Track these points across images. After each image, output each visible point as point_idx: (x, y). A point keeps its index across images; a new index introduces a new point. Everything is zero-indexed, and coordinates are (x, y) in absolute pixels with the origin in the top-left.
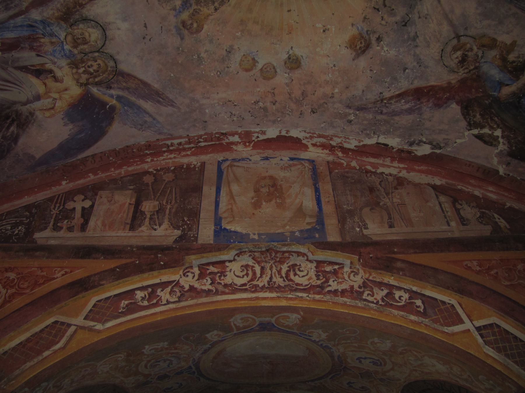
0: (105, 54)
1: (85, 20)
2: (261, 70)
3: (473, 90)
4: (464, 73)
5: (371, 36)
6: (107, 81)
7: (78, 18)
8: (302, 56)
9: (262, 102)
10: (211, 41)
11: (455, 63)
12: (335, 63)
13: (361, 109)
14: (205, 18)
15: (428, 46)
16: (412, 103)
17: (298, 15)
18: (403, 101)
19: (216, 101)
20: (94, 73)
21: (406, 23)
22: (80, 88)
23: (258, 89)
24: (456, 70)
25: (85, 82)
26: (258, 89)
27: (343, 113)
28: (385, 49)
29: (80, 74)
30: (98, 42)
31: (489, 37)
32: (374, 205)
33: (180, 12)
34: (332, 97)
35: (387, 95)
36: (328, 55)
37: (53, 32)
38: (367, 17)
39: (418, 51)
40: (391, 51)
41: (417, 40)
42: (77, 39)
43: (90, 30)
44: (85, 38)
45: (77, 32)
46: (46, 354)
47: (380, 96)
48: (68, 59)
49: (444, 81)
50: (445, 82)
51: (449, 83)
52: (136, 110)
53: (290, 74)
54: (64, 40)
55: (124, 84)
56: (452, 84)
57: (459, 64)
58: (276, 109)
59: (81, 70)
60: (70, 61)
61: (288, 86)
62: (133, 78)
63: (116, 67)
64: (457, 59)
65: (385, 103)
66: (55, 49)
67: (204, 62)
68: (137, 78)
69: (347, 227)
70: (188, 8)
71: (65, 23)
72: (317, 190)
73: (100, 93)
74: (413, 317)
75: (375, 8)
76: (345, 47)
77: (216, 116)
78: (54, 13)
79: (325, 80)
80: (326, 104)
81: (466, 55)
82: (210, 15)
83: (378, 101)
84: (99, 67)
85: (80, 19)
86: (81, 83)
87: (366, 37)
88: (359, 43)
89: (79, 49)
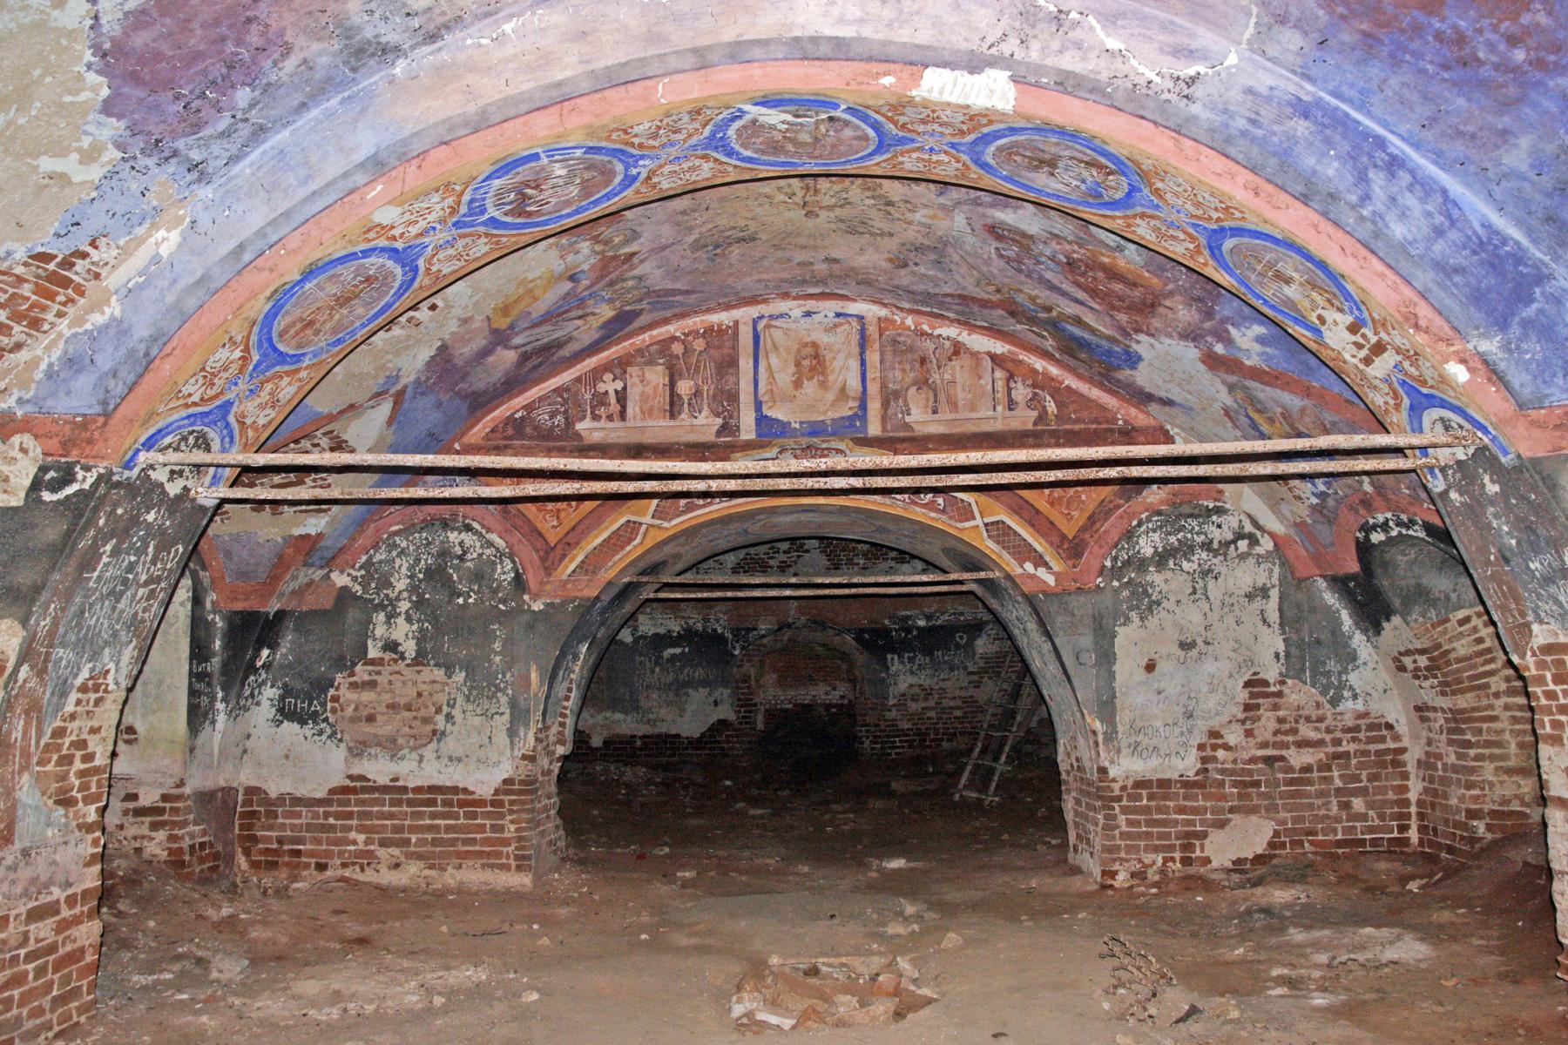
32: (923, 383)
46: (628, 548)
69: (890, 412)
72: (863, 363)
74: (933, 515)
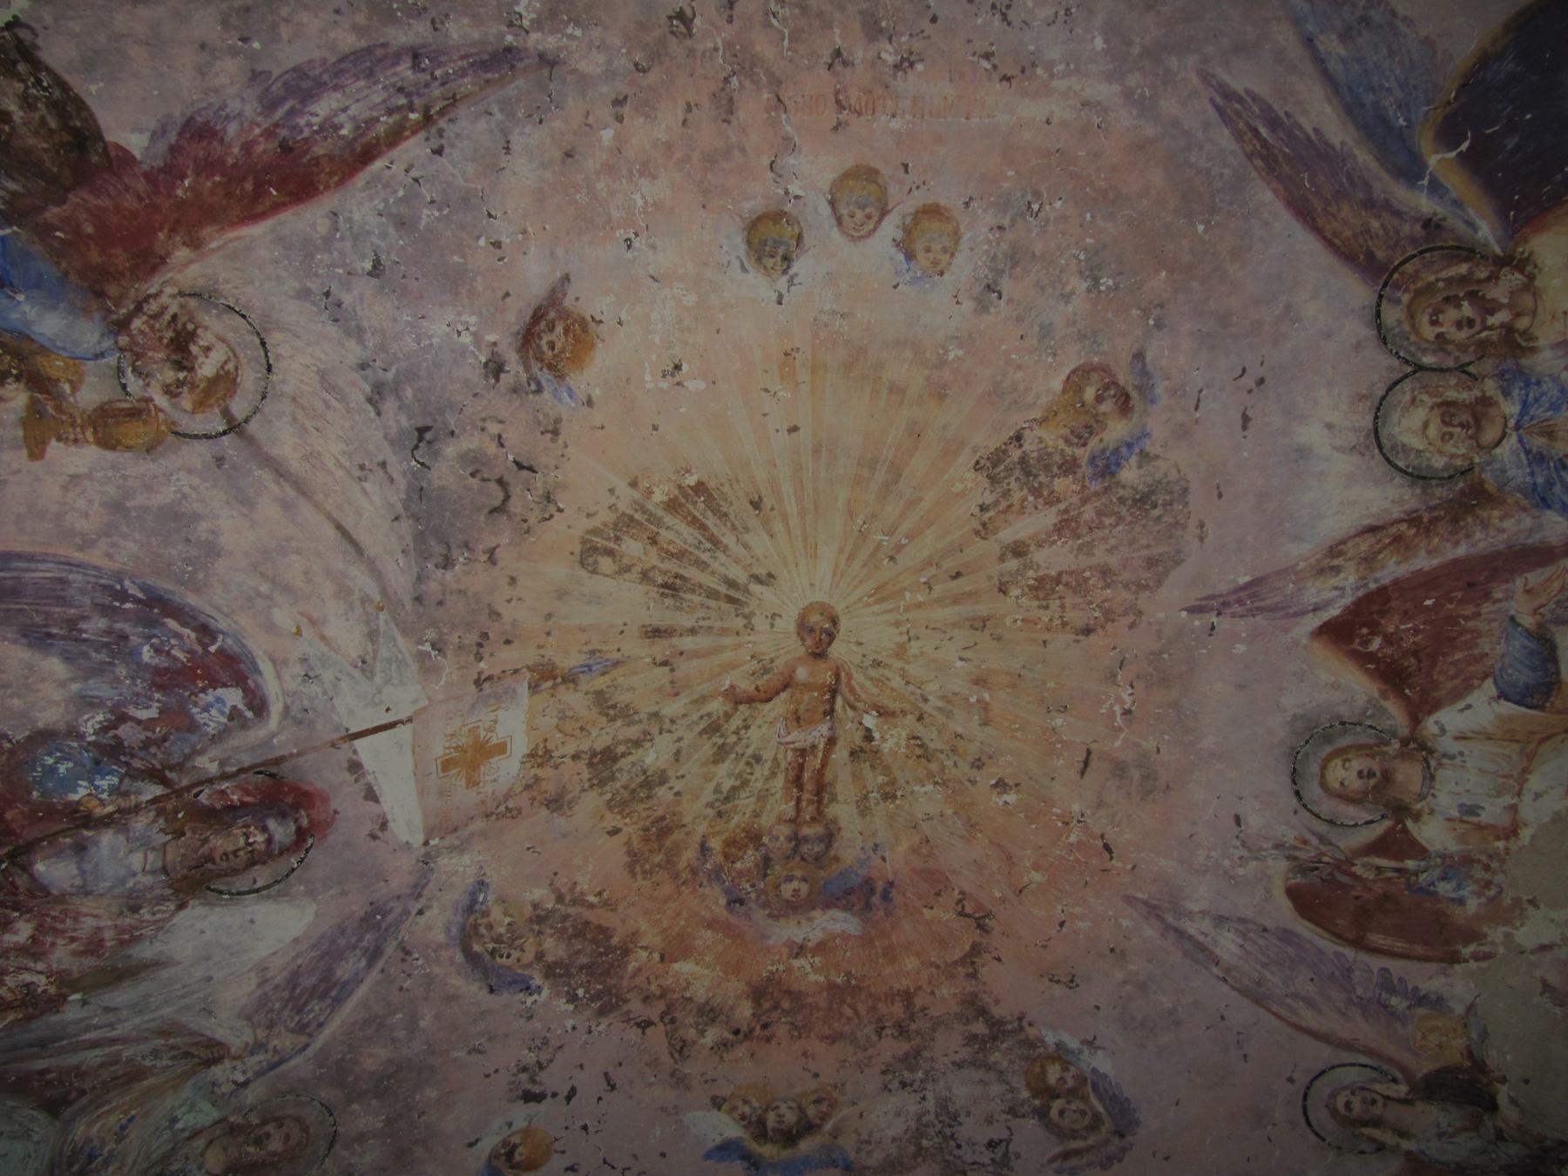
0: (1401, 354)
1: (1419, 477)
2: (884, 213)
3: (89, 229)
4: (156, 296)
5: (524, 376)
6: (1428, 255)
7: (1440, 489)
8: (744, 269)
9: (884, 62)
10: (1046, 331)
11: (206, 328)
12: (629, 255)
13: (500, 61)
14: (1056, 414)
15: (323, 375)
16: (309, 125)
17: (765, 415)
18: (344, 132)
19: (1060, 85)
20: (1461, 295)
21: (420, 439)
22: (1531, 254)
23: (896, 124)
24: (192, 302)
25: (1505, 270)
26: (896, 124)
27: (567, 24)
28: (466, 339)
29: (1510, 306)
30: (1408, 397)
31: (129, 448)
33: (1129, 446)
34: (619, 102)
35: (414, 148)
36: (655, 284)
37: (1530, 464)
38: (549, 436)
39: (354, 351)
40: (447, 334)
41: (367, 388)
42: (1468, 423)
43: (1417, 443)
44: (1444, 422)
45: (1459, 449)
47: (441, 136)
48: (1526, 371)
49: (219, 248)
50: (213, 245)
51: (195, 244)
52: (1369, 98)
53: (782, 192)
54: (1508, 431)
55: (1375, 225)
56: (184, 243)
57: (190, 327)
58: (831, 27)
59: (1502, 317)
60: (1523, 361)
61: (787, 139)
62: (1336, 241)
63: (1381, 297)
64: (206, 344)
65: (412, 109)
66: (1549, 414)
67: (1082, 257)
68: (1325, 238)
70: (1103, 451)
71: (1482, 483)
73: (1471, 212)
75: (531, 469)
76: (601, 322)
77: (1068, 12)
78: (1502, 519)
79: (654, 177)
80: (636, 65)
81: (179, 366)
82: (1043, 421)
83: (442, 113)
84: (1436, 315)
85: (1434, 482)
86: (1522, 271)
87: (541, 369)
88: (558, 346)
89: (1476, 393)
